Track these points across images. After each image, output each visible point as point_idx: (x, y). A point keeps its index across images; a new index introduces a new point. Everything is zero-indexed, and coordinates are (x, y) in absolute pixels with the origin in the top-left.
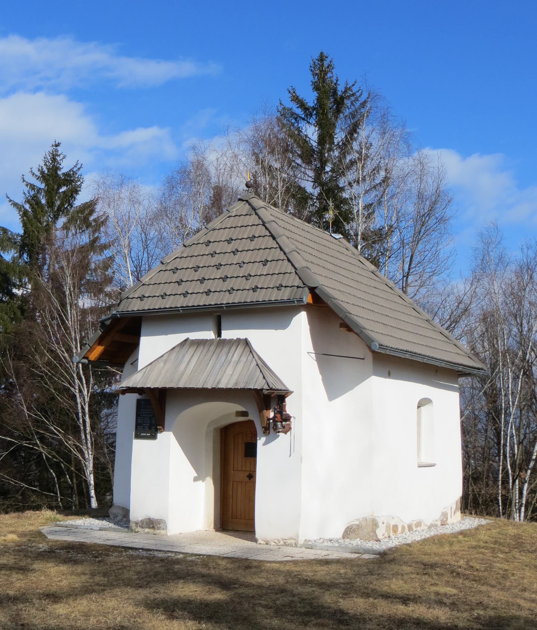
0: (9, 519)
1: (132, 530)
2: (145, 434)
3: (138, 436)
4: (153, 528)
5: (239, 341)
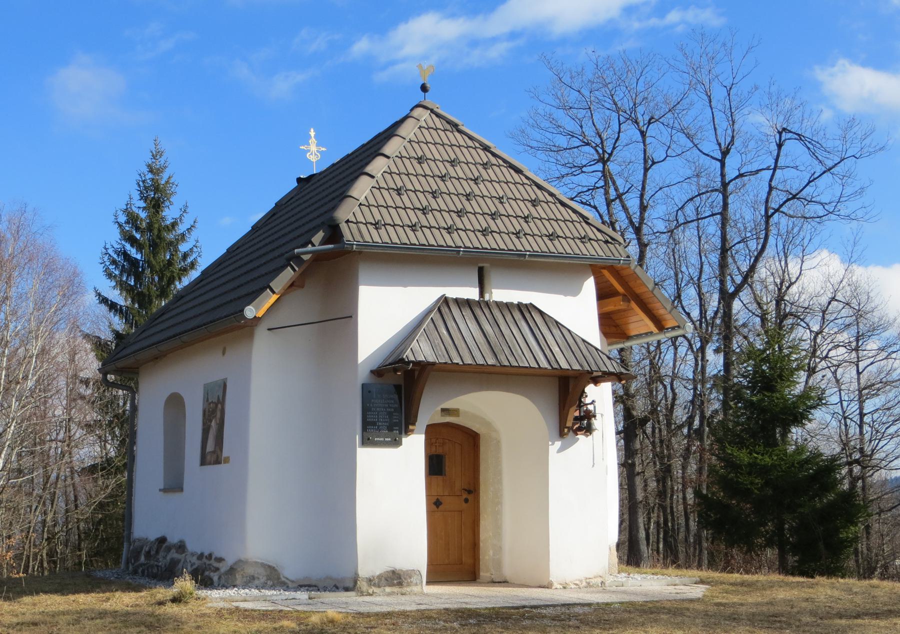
0: (6, 606)
1: (362, 592)
2: (382, 439)
3: (367, 442)
4: (400, 584)
5: (520, 306)
